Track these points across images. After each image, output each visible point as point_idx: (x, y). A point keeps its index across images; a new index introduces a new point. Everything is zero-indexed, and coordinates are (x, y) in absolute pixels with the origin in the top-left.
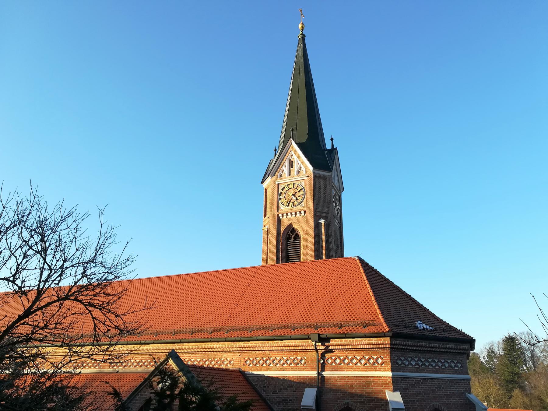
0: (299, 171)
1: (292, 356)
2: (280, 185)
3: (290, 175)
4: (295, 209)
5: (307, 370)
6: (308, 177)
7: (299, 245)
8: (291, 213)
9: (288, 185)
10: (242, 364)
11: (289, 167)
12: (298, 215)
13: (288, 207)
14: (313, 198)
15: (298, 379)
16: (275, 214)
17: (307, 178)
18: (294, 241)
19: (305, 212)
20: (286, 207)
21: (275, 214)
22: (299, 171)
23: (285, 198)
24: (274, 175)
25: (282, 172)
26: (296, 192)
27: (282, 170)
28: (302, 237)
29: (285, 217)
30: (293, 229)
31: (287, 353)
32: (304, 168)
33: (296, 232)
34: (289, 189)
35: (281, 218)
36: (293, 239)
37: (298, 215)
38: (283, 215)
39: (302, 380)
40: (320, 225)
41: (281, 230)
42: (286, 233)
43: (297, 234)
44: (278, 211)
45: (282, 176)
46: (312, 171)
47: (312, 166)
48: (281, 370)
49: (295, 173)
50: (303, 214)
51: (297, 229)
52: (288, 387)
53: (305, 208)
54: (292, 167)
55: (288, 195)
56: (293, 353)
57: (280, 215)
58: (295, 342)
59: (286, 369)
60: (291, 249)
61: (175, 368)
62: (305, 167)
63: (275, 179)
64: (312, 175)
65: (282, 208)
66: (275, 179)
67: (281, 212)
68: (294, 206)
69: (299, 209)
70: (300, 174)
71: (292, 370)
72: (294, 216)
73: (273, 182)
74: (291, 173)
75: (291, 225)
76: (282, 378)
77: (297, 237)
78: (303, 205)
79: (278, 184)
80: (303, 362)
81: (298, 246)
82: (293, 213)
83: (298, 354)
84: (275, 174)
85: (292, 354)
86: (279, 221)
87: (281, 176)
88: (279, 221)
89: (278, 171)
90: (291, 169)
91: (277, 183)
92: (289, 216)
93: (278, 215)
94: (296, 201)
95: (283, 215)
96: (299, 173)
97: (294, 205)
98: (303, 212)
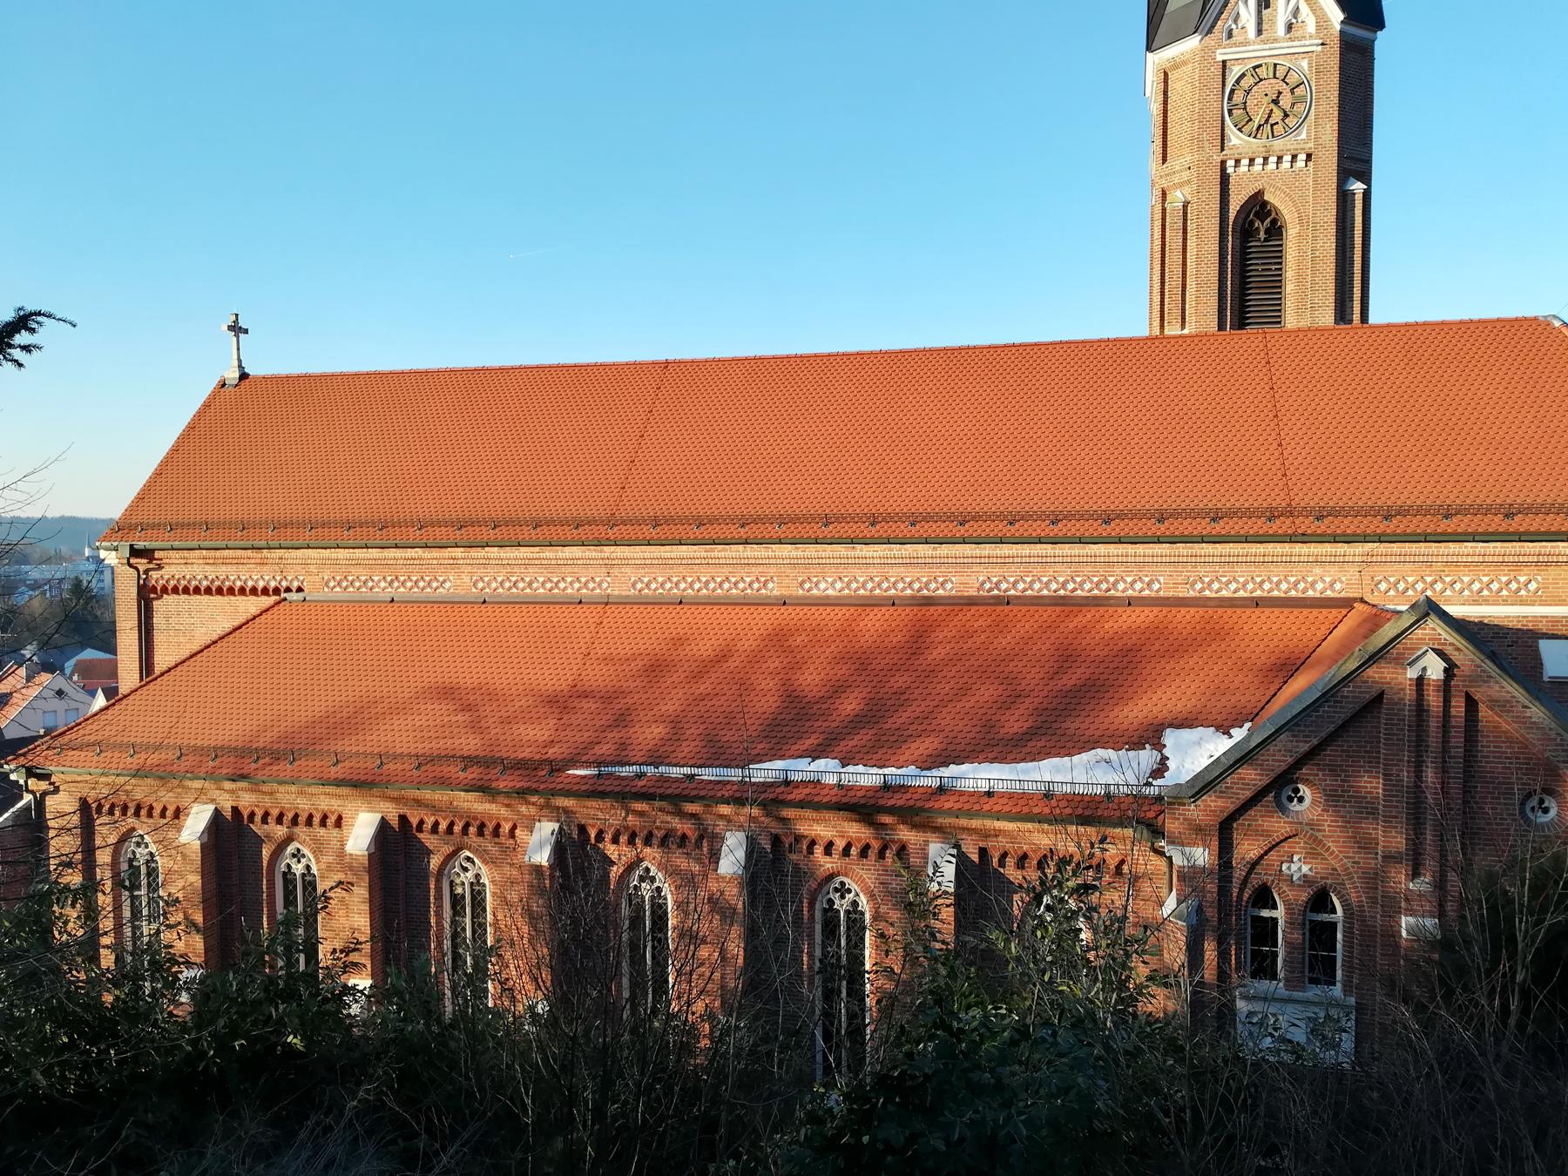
0: (1294, 21)
1: (1505, 575)
2: (1228, 64)
3: (1260, 32)
4: (1278, 144)
5: (1543, 603)
6: (1323, 44)
7: (1279, 255)
8: (1266, 159)
9: (1255, 68)
10: (1367, 589)
11: (1259, 5)
12: (1286, 165)
13: (1255, 137)
14: (1336, 113)
15: (1519, 621)
16: (1215, 157)
17: (1320, 48)
18: (1266, 240)
19: (1309, 157)
20: (1251, 139)
21: (1215, 157)
22: (1294, 21)
23: (1245, 109)
24: (1210, 31)
25: (1236, 21)
26: (1280, 93)
27: (1234, 14)
28: (1292, 233)
29: (1243, 168)
30: (1265, 204)
31: (1492, 568)
32: (1310, 13)
33: (1273, 215)
34: (1261, 80)
35: (1230, 170)
36: (1262, 235)
37: (1286, 165)
38: (1238, 162)
39: (1530, 624)
40: (1349, 198)
41: (1231, 207)
42: (1243, 216)
43: (1274, 221)
44: (1222, 150)
45: (1235, 32)
46: (1338, 27)
47: (1344, 10)
48: (1476, 603)
49: (1281, 30)
50: (1300, 163)
51: (1275, 208)
52: (1492, 637)
53: (1312, 145)
54: (1267, 6)
55: (1255, 101)
56: (1506, 568)
57: (1231, 163)
58: (1523, 547)
59: (1486, 602)
60: (1256, 266)
61: (1444, 635)
62: (1314, 11)
63: (1213, 43)
64: (1337, 41)
65: (1235, 139)
66: (1213, 43)
67: (1232, 152)
68: (1273, 137)
69: (1292, 147)
70: (1293, 34)
71: (1505, 602)
72: (1272, 166)
73: (1206, 53)
74: (1265, 26)
75: (1260, 193)
76: (1476, 620)
77: (1276, 230)
78: (1303, 136)
79: (1224, 62)
80: (1532, 587)
81: (1278, 256)
82: (1273, 159)
83: (1521, 570)
84: (1213, 26)
85: (1504, 570)
86: (1224, 179)
87: (1230, 35)
88: (1224, 179)
89: (1223, 16)
90: (1264, 12)
91: (1220, 58)
92: (1257, 168)
93: (1223, 163)
94: (1281, 123)
95: (1238, 162)
96: (1290, 27)
97: (1275, 134)
98: (1302, 157)
